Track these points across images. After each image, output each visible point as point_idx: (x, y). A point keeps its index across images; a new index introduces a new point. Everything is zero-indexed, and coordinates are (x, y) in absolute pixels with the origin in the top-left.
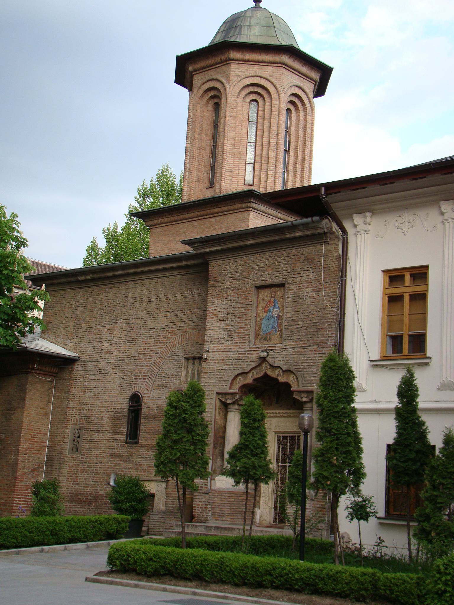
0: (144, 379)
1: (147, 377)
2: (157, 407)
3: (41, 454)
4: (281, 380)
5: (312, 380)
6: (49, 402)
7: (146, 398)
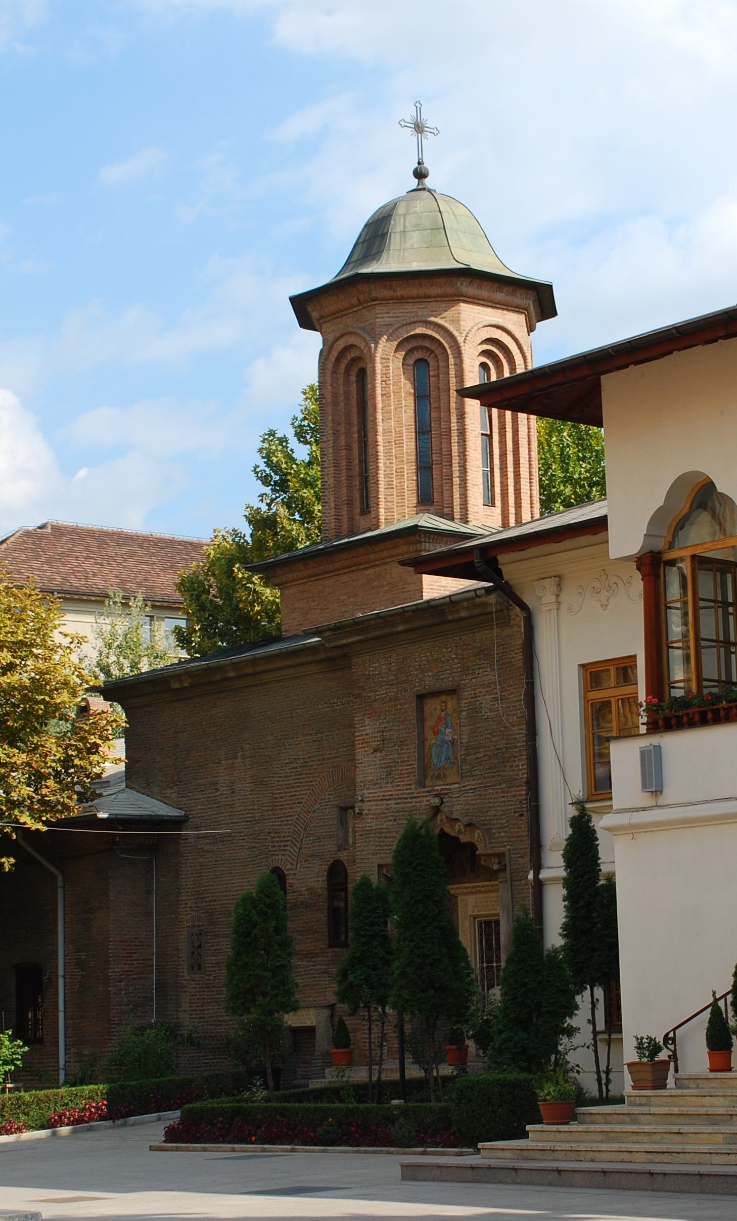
0: (285, 846)
1: (289, 843)
2: (308, 890)
3: (146, 978)
4: (464, 839)
5: (502, 837)
6: (150, 892)
7: (291, 877)
